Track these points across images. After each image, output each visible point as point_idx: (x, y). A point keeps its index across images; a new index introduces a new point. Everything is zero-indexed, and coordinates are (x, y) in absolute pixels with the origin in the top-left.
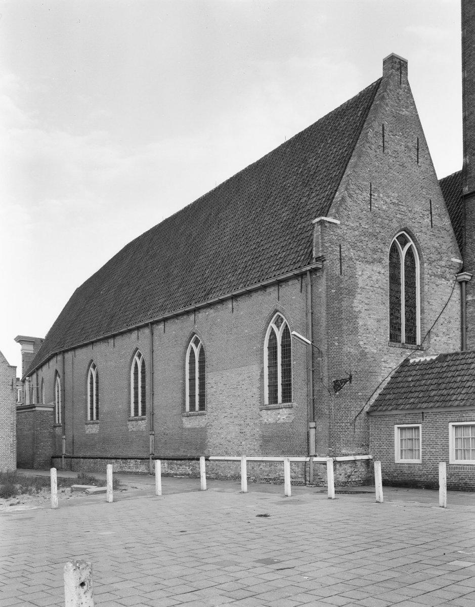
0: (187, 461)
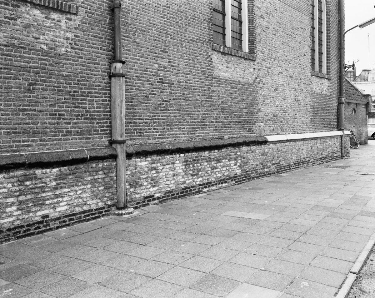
0: (230, 149)
